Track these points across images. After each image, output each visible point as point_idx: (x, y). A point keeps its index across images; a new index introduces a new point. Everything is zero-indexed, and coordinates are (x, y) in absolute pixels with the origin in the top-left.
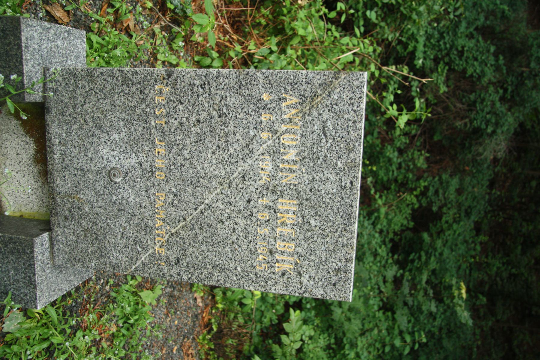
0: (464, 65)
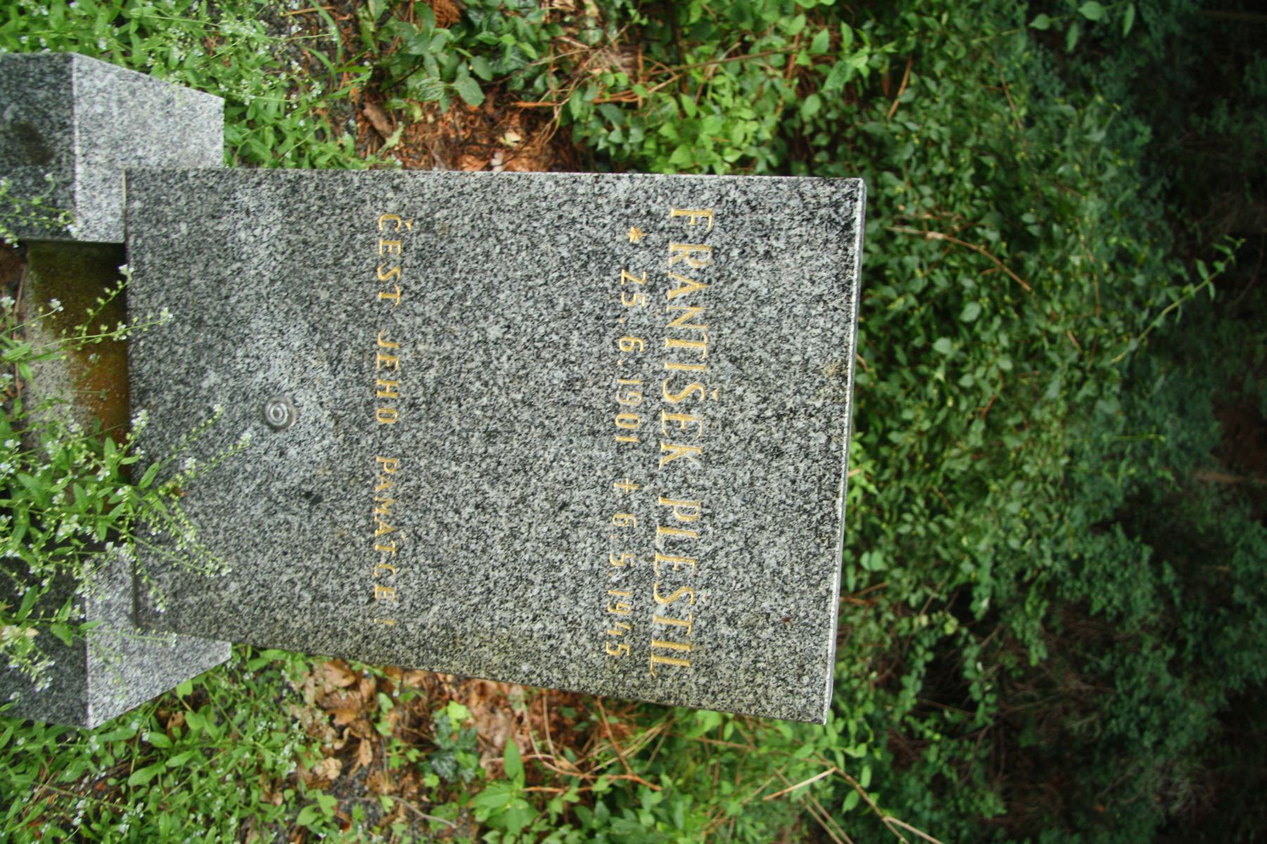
0: (1085, 590)
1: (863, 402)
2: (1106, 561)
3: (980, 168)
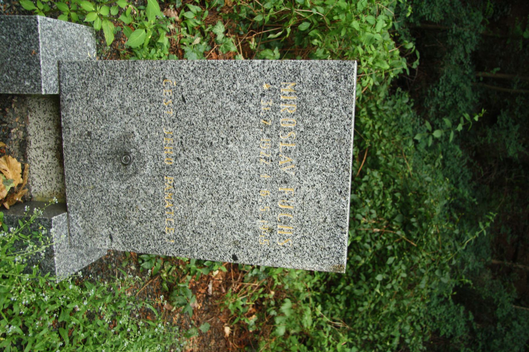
0: (438, 327)
1: (348, 295)
2: (446, 315)
3: (395, 199)
